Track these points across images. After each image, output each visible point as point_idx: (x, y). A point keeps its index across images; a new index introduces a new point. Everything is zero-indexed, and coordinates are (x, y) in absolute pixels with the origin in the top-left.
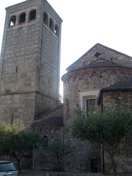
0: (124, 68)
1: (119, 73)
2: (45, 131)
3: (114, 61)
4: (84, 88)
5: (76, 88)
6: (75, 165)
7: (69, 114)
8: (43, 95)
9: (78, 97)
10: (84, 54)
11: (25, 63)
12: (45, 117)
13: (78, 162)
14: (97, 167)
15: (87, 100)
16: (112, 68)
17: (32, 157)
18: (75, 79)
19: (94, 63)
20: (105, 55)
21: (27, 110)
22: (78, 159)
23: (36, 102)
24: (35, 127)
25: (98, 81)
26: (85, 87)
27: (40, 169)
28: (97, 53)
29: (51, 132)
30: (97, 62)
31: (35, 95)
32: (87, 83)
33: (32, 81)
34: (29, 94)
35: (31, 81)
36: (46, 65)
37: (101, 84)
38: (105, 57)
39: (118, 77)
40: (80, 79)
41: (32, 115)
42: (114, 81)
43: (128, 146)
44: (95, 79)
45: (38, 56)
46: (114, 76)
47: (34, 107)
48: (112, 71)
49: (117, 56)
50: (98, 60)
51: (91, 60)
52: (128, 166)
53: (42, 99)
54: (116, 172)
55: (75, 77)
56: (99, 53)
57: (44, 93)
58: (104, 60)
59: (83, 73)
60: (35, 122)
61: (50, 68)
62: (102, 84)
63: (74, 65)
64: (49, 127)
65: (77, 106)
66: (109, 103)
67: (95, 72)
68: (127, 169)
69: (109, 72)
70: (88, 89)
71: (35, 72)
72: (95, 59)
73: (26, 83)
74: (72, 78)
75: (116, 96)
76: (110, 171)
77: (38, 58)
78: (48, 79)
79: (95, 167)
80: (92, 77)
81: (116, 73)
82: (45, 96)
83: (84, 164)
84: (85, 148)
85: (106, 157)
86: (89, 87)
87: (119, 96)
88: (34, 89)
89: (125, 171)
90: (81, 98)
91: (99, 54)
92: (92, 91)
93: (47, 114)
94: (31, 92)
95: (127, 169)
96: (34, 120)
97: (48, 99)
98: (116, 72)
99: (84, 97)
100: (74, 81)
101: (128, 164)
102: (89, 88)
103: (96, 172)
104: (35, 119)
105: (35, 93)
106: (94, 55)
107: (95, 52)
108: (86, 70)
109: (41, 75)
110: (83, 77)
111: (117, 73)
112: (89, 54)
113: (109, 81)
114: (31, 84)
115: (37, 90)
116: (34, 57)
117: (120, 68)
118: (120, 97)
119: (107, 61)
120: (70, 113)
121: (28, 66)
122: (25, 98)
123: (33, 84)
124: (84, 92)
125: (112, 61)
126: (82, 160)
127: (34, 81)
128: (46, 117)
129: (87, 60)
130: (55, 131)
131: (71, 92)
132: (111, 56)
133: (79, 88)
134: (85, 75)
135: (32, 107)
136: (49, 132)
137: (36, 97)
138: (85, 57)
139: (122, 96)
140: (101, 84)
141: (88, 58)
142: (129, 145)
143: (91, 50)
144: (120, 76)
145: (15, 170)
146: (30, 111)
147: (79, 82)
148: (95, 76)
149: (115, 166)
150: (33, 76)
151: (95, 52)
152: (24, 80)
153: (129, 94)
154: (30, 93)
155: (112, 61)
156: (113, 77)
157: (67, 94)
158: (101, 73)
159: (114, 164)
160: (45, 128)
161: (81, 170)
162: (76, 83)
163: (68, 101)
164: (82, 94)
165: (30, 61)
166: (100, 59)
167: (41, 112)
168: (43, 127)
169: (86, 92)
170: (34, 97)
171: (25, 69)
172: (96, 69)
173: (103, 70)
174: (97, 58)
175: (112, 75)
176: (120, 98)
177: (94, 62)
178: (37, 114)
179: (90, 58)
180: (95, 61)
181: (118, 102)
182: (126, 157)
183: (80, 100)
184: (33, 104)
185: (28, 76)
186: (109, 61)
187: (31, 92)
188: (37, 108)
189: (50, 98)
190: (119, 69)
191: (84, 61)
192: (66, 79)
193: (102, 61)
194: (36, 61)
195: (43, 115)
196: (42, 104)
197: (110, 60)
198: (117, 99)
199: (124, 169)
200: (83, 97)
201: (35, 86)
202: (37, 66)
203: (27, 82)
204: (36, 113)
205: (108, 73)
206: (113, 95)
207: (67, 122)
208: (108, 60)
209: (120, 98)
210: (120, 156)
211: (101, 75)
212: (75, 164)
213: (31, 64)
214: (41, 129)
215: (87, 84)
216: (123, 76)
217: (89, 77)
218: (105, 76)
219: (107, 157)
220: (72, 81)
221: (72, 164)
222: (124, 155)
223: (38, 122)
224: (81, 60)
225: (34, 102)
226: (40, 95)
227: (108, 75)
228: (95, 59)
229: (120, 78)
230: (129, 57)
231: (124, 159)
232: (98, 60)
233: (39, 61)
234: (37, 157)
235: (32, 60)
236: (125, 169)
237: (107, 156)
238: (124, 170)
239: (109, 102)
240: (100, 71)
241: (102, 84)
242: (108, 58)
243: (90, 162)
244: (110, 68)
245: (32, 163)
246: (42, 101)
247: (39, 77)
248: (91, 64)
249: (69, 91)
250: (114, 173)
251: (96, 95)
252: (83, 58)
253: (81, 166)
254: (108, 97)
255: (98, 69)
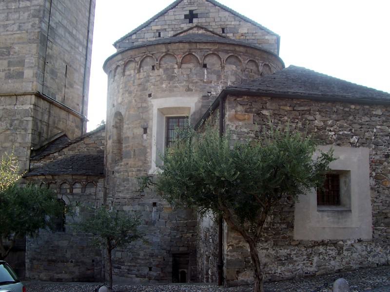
0: (257, 51)
1: (245, 61)
2: (60, 188)
3: (228, 35)
4: (162, 87)
5: (143, 87)
6: (135, 266)
7: (120, 149)
8: (51, 103)
9: (146, 109)
10: (159, 11)
11: (7, 20)
12: (56, 154)
13: (143, 259)
14: (185, 270)
15: (168, 119)
16: (231, 48)
17: (25, 250)
18: (140, 67)
19: (182, 35)
20: (208, 20)
21: (11, 138)
22: (142, 253)
23: (35, 119)
24: (36, 178)
25: (196, 74)
26: (164, 86)
27: (45, 278)
28: (191, 12)
29: (75, 191)
30: (189, 34)
31: (33, 103)
32: (171, 78)
33: (26, 66)
34: (18, 97)
35: (24, 66)
36: (61, 31)
37: (204, 82)
38: (209, 22)
39: (243, 71)
40: (153, 67)
41: (25, 150)
42: (233, 79)
43: (278, 223)
44: (191, 71)
45: (44, 6)
46: (234, 67)
47: (30, 131)
48: (230, 54)
49: (238, 23)
50: (191, 28)
51: (176, 27)
52: (276, 266)
53: (49, 112)
54: (260, 280)
55: (142, 62)
56: (194, 12)
57: (55, 98)
58: (206, 30)
59: (163, 53)
60: (31, 167)
61: (70, 39)
62: (206, 83)
63: (135, 35)
64: (69, 178)
65: (143, 129)
66: (241, 123)
67: (190, 54)
68: (275, 273)
69: (224, 56)
70: (174, 91)
71: (34, 45)
72: (185, 26)
73: (9, 70)
74: (132, 65)
75: (256, 107)
76: (237, 278)
77: (44, 11)
78: (64, 65)
79: (180, 270)
80: (184, 66)
81: (240, 61)
82: (56, 105)
83: (157, 266)
84: (160, 229)
85: (229, 246)
86: (176, 87)
87: (263, 108)
88: (32, 86)
89: (270, 278)
90: (155, 112)
91: (196, 16)
92: (181, 96)
93: (63, 148)
94: (24, 94)
95: (273, 272)
96: (28, 162)
97: (63, 114)
98: (239, 57)
99: (161, 111)
100: (139, 72)
101: (276, 263)
102: (175, 89)
103: (183, 280)
104: (32, 159)
105: (33, 97)
106: (183, 17)
107: (187, 10)
108: (169, 47)
109: (49, 53)
110: (162, 62)
111: (242, 60)
112: (171, 12)
113: (223, 78)
114: (23, 73)
115: (39, 89)
116: (32, 8)
117: (248, 49)
118: (266, 111)
119: (211, 32)
120: (124, 145)
121: (16, 27)
122: (8, 107)
123: (28, 73)
124: (162, 97)
125: (223, 35)
126: (152, 255)
127: (32, 67)
128: (61, 155)
129: (166, 27)
130: (84, 187)
131: (130, 96)
132: (223, 23)
133: (151, 89)
134: (168, 58)
135: (26, 130)
136: (68, 191)
137: (35, 105)
138: (162, 18)
139: (269, 107)
140: (204, 82)
141: (168, 22)
142: (281, 219)
143: (177, 5)
144: (246, 68)
145: (14, 283)
146: (19, 140)
147: (151, 74)
148: (189, 62)
149: (257, 264)
150: (30, 53)
151: (187, 10)
152: (5, 62)
153: (286, 105)
154: (21, 95)
155: (223, 35)
156: (231, 68)
157: (120, 100)
158: (206, 57)
159: (257, 262)
160: (59, 181)
161: (150, 279)
162: (142, 75)
163: (119, 117)
164: (157, 104)
165: (21, 18)
166: (197, 26)
167: (47, 142)
168: (53, 179)
169: (168, 98)
170: (32, 106)
171: (10, 37)
172: (194, 46)
173: (210, 49)
174: (191, 25)
175: (230, 63)
176: (265, 112)
177: (182, 33)
178: (38, 147)
179: (174, 23)
180: (185, 31)
181: (262, 122)
182: (273, 247)
183: (151, 116)
184: (27, 124)
185: (15, 53)
186: (218, 33)
187: (24, 94)
188: (37, 133)
189: (68, 111)
190: (246, 52)
191: (159, 27)
192: (118, 66)
193: (201, 32)
194: (37, 19)
195: (54, 151)
196: (48, 125)
197: (219, 31)
198: (258, 114)
199: (269, 273)
200: (158, 109)
201: (35, 79)
202: (39, 30)
203: (12, 69)
204: (33, 145)
205: (220, 59)
206: (251, 105)
207: (116, 168)
208: (215, 31)
209: (265, 112)
210: (261, 245)
211: (205, 62)
212: (134, 264)
213: (26, 25)
214: (49, 184)
215: (170, 80)
216: (254, 68)
217: (177, 64)
218: (214, 65)
219: (231, 248)
220: (132, 72)
221: (126, 264)
222: (269, 242)
223: (39, 167)
224: (151, 25)
225: (31, 119)
226: (46, 102)
227: (220, 63)
228: (185, 26)
229: (247, 73)
230: (263, 30)
231: (269, 251)
232: (191, 28)
233: (47, 20)
234: (38, 250)
235: (26, 14)
236: (270, 272)
237: (230, 244)
238: (267, 275)
239: (240, 120)
240: (203, 53)
241: (206, 83)
242: (216, 27)
243: (171, 259)
244: (227, 48)
245: (24, 264)
246: (49, 116)
247: (45, 59)
248: (175, 36)
249: (123, 94)
250: (257, 280)
251: (189, 108)
252: (157, 20)
253: (150, 269)
254: (239, 108)
255: (198, 46)
